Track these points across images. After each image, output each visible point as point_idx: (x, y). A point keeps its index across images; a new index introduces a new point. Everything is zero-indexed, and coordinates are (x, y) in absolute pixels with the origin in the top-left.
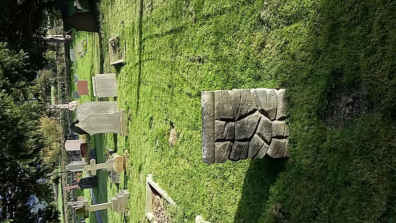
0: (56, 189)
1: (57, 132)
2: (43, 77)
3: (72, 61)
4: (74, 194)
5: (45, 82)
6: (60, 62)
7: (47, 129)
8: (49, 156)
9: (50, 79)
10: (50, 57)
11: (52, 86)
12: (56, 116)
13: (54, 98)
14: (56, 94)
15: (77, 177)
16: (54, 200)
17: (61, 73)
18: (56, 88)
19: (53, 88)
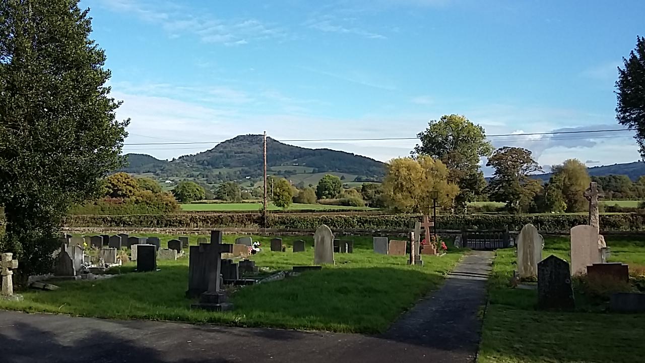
0: (335, 202)
2: (522, 191)
3: (132, 246)
4: (388, 232)
8: (395, 194)
10: (555, 204)
12: (456, 207)
15: (436, 241)
16: (318, 199)
19: (502, 204)
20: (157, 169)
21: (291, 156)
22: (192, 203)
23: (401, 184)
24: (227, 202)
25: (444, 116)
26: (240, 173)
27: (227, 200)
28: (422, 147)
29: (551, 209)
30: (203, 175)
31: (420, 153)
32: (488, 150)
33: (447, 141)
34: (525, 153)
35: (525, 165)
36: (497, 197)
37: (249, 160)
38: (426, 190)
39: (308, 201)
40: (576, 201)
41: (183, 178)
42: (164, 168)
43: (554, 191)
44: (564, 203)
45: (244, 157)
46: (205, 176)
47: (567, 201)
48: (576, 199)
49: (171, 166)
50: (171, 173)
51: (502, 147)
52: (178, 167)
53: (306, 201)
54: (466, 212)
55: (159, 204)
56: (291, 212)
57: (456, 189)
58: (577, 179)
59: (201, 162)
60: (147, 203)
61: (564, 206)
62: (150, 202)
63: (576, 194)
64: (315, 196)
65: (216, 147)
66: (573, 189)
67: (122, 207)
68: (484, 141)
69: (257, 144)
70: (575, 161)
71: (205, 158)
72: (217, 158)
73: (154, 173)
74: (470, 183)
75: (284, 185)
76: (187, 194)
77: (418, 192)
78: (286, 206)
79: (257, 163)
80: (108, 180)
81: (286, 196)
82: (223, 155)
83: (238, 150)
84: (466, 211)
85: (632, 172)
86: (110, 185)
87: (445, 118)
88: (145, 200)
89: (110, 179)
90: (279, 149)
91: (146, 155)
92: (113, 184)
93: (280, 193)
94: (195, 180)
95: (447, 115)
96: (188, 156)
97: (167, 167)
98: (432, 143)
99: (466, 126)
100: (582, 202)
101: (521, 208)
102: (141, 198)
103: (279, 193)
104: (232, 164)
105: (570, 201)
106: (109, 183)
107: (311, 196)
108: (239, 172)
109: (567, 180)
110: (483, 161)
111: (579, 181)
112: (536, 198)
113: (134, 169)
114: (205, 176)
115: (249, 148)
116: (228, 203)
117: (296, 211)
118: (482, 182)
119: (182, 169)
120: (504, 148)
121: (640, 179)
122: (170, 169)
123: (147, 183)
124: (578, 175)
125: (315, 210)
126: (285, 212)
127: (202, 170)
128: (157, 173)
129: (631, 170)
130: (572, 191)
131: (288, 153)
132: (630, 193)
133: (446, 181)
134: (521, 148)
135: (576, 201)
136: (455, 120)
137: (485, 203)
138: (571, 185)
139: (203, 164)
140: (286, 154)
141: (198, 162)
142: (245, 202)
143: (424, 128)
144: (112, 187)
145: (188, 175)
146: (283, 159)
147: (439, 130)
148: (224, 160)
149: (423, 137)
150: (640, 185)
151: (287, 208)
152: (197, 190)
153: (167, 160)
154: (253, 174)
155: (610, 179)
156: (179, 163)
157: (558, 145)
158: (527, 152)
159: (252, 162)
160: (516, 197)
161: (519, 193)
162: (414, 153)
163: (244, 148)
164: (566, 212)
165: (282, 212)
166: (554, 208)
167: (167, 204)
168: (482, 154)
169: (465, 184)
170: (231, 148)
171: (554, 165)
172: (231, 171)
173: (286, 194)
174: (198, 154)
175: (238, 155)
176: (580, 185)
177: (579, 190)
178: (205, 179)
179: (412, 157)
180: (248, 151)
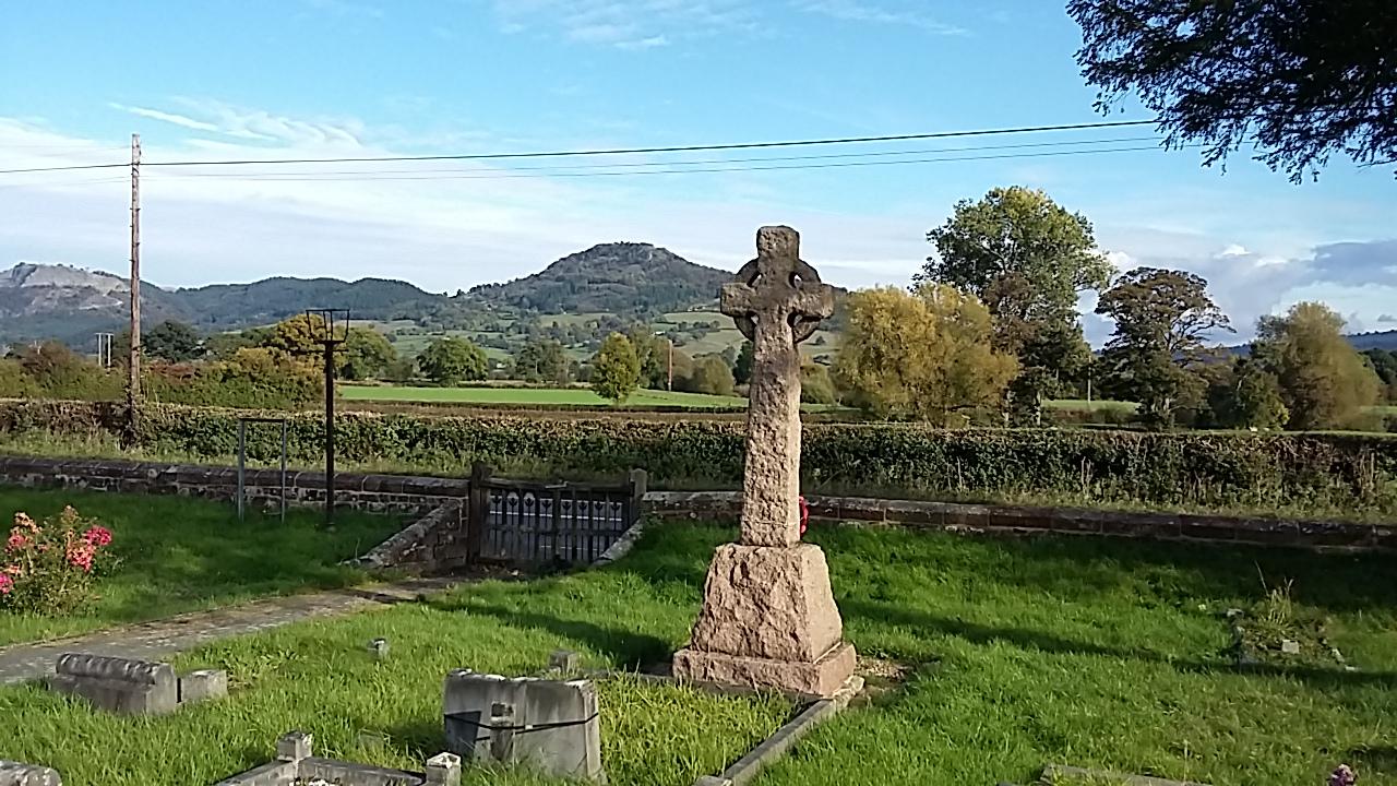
1: (950, 410)
2: (1177, 375)
5: (1155, 382)
6: (1287, 460)
7: (966, 377)
8: (861, 373)
9: (1167, 401)
10: (1259, 409)
11: (1138, 405)
12: (1015, 410)
13: (1094, 410)
14: (1108, 416)
17: (1202, 459)
18: (1131, 419)
19: (1131, 407)
20: (423, 312)
21: (709, 292)
22: (459, 386)
23: (877, 350)
24: (537, 385)
25: (993, 190)
26: (599, 326)
27: (536, 382)
28: (941, 266)
29: (1251, 421)
30: (520, 327)
31: (938, 277)
32: (1099, 274)
33: (1002, 250)
34: (1193, 283)
35: (1188, 313)
36: (1120, 390)
37: (620, 297)
38: (936, 366)
39: (715, 387)
40: (1313, 404)
41: (478, 333)
42: (437, 311)
43: (1259, 376)
44: (1283, 406)
45: (608, 292)
46: (523, 330)
47: (1292, 402)
48: (1314, 399)
49: (454, 307)
50: (451, 322)
51: (1136, 269)
52: (467, 310)
53: (710, 388)
54: (1039, 423)
55: (281, 382)
56: (632, 411)
57: (1011, 366)
58: (1319, 351)
59: (516, 300)
60: (253, 379)
61: (1282, 415)
62: (260, 377)
63: (1315, 387)
64: (733, 378)
65: (549, 267)
66: (1307, 373)
67: (191, 387)
68: (1094, 253)
69: (637, 263)
70: (1316, 308)
71: (525, 291)
72: (550, 292)
73: (417, 320)
74: (1050, 352)
75: (618, 347)
76: (449, 365)
77: (916, 370)
78: (621, 396)
79: (635, 304)
80: (279, 329)
81: (621, 372)
82: (564, 287)
83: (597, 276)
84: (1039, 419)
86: (282, 341)
87: (995, 195)
88: (248, 369)
89: (282, 327)
90: (685, 276)
91: (401, 282)
92: (288, 340)
93: (608, 365)
94: (501, 337)
95: (1001, 188)
96: (489, 285)
97: (444, 309)
98: (962, 255)
99: (1045, 215)
100: (1329, 405)
101: (1173, 415)
102: (239, 365)
103: (605, 366)
104: (582, 306)
105: (1299, 403)
106: (279, 335)
107: (722, 378)
108: (595, 324)
109: (1293, 352)
110: (1086, 303)
111: (1325, 354)
112: (1216, 393)
113: (375, 312)
114: (523, 330)
115: (620, 271)
116: (539, 388)
117: (645, 409)
118: (1076, 350)
119: (476, 314)
120: (1141, 270)
122: (450, 312)
123: (365, 339)
124: (1321, 341)
125: (687, 408)
126: (619, 411)
127: (517, 317)
128: (422, 320)
130: (1305, 380)
131: (704, 284)
133: (988, 347)
134: (1182, 270)
135: (1313, 404)
136: (1019, 198)
137: (1104, 404)
138: (1306, 363)
139: (519, 305)
140: (699, 286)
141: (510, 299)
142: (575, 387)
143: (942, 216)
144: (286, 345)
145: (487, 327)
146: (691, 297)
147: (979, 222)
148: (566, 297)
149: (943, 240)
151: (625, 401)
152: (472, 356)
153: (445, 294)
154: (626, 329)
156: (469, 301)
157: (1323, 279)
158: (1196, 281)
159: (625, 302)
160: (1162, 389)
161: (1168, 379)
162: (921, 278)
163: (608, 272)
164: (1286, 428)
165: (613, 410)
166: (1256, 419)
167: (300, 383)
168: (1088, 283)
169: (1037, 354)
170: (580, 271)
171: (1264, 314)
172: (580, 320)
173: (622, 368)
174: (510, 282)
175: (596, 286)
176: (1326, 364)
177: (1323, 378)
178: (523, 336)
179: (917, 287)
180: (616, 279)
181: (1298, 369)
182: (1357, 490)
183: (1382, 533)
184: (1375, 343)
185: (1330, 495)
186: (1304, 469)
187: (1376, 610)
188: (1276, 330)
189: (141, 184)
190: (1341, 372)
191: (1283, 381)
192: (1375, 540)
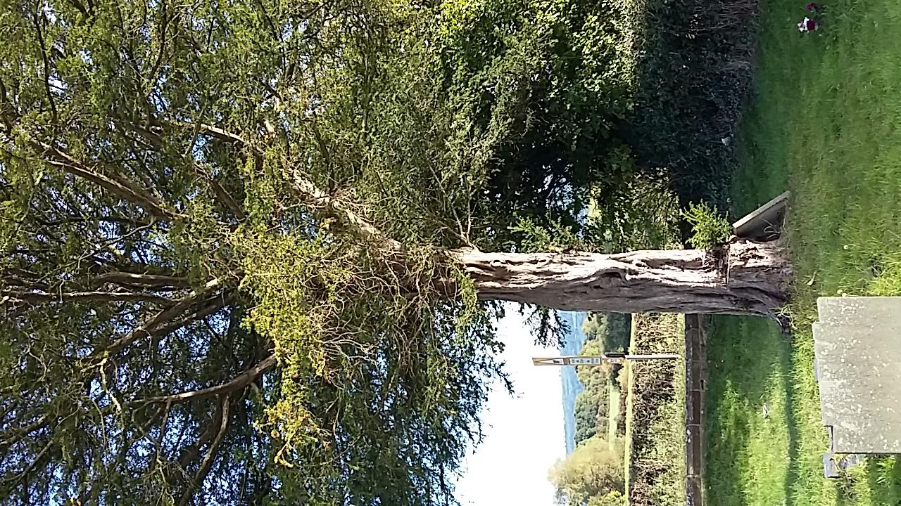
47: (607, 489)
66: (589, 479)
85: (573, 386)
105: (607, 485)
109: (575, 486)
121: (581, 381)
124: (570, 470)
129: (570, 386)
132: (600, 394)
135: (608, 477)
150: (589, 381)
155: (580, 417)
176: (584, 468)
181: (586, 485)
182: (664, 470)
183: (691, 472)
184: (571, 438)
185: (667, 486)
186: (651, 500)
187: (742, 482)
188: (561, 495)
189: (803, 445)
190: (589, 459)
191: (594, 494)
192: (696, 476)
